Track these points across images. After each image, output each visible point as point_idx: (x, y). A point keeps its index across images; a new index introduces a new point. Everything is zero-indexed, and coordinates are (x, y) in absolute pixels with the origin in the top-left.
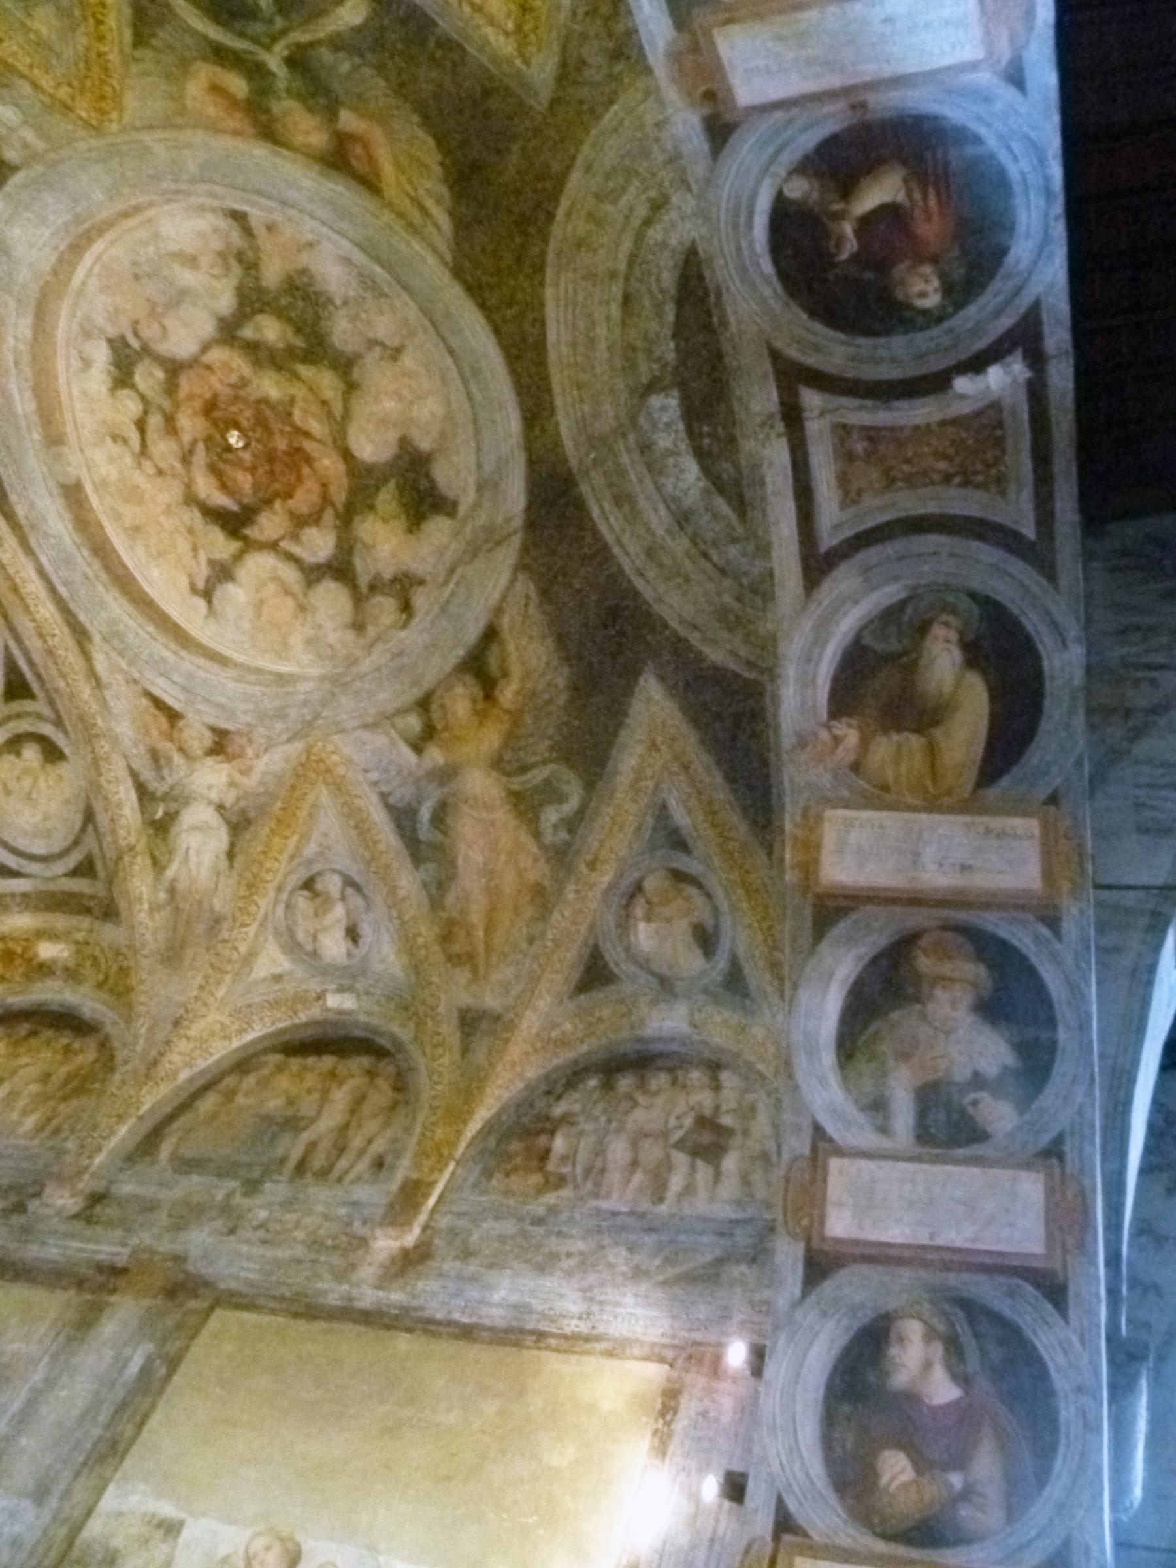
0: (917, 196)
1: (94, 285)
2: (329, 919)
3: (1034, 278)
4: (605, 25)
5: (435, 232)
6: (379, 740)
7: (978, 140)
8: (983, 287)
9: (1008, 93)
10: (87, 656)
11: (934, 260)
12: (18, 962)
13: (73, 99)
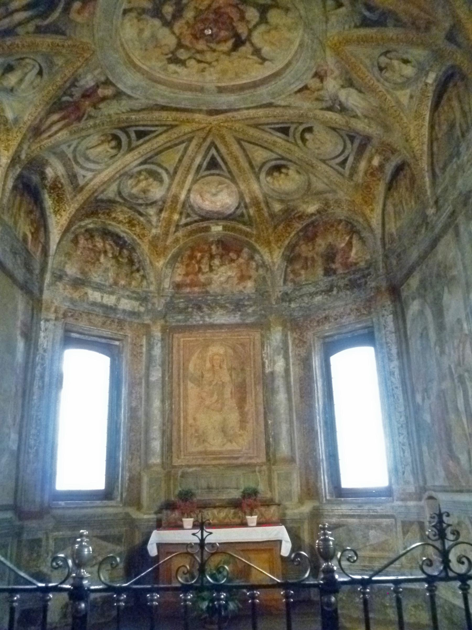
1: (148, 64)
2: (397, 68)
6: (333, 19)
10: (277, 106)
12: (375, 172)
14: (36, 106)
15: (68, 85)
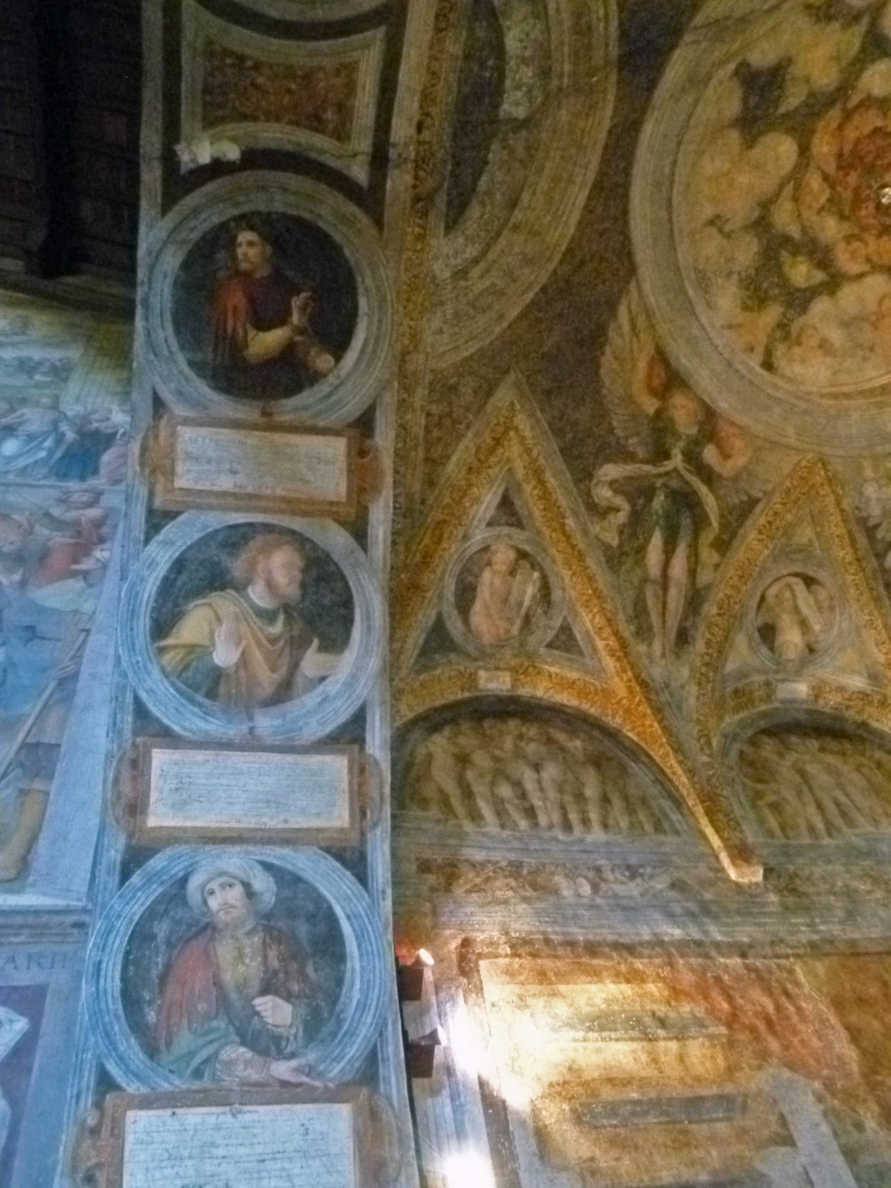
0: (240, 332)
3: (164, 234)
4: (452, 412)
5: (633, 307)
7: (191, 363)
8: (203, 238)
9: (166, 395)
11: (238, 273)
13: (822, 485)
14: (871, 624)
15: (863, 541)
